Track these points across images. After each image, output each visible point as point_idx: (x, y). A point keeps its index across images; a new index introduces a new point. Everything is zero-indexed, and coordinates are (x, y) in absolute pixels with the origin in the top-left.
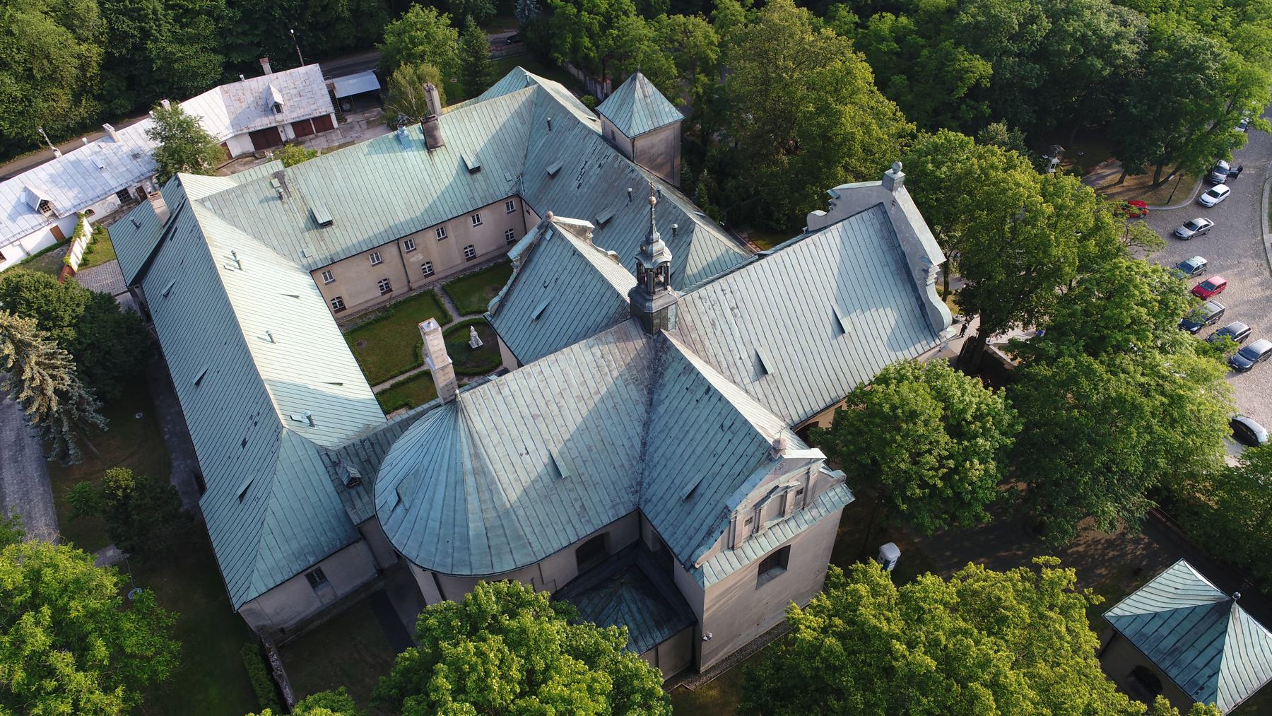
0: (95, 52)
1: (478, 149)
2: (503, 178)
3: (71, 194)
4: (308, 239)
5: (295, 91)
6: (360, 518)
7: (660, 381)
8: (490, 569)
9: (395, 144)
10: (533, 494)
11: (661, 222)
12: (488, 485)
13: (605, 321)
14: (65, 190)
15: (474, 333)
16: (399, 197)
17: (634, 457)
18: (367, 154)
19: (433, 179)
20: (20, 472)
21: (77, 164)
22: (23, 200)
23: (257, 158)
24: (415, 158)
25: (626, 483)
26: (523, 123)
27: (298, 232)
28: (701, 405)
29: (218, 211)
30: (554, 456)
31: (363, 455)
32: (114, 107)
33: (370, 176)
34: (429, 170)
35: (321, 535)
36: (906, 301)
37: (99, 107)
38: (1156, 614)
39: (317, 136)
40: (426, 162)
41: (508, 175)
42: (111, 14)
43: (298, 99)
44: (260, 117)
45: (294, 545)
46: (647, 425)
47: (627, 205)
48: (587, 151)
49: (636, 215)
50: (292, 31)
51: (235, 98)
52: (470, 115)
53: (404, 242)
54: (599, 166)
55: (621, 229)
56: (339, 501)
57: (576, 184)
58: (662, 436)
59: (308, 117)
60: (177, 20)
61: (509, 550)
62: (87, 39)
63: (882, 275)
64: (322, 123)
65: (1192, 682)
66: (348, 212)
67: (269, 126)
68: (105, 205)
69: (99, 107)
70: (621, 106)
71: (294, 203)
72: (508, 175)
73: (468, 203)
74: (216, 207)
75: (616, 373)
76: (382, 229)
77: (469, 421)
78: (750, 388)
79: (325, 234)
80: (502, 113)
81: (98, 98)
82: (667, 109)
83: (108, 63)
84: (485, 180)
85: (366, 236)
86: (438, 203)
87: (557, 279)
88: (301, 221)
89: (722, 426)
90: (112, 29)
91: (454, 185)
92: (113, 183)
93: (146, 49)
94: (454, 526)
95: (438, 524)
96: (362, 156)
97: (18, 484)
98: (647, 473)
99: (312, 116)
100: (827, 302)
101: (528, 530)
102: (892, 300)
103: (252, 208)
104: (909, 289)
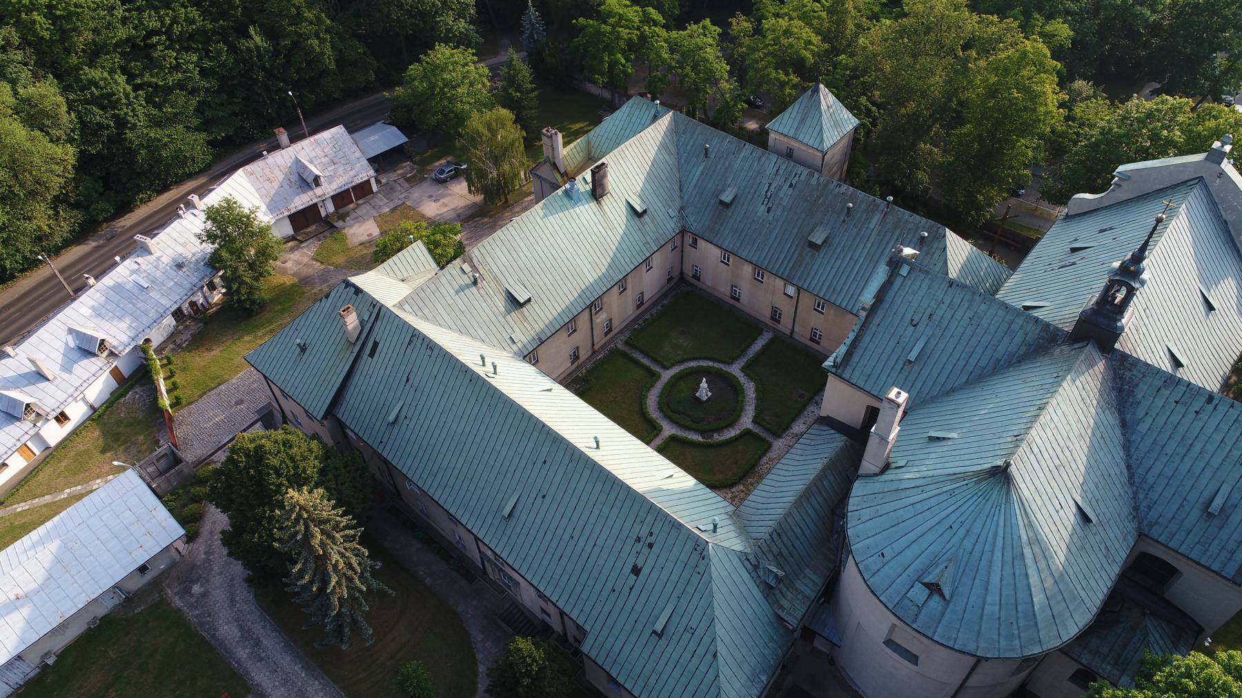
0: (69, 153)
3: (124, 325)
6: (794, 617)
7: (1131, 399)
8: (1059, 640)
9: (566, 200)
10: (1073, 549)
13: (1023, 349)
14: (115, 322)
15: (704, 385)
17: (1125, 483)
18: (544, 217)
19: (608, 230)
20: (276, 671)
21: (118, 288)
22: (72, 344)
23: (301, 242)
24: (586, 211)
26: (670, 154)
27: (501, 318)
28: (1204, 416)
29: (420, 313)
30: (1080, 504)
32: (94, 213)
33: (552, 240)
34: (602, 221)
35: (764, 649)
37: (79, 216)
39: (358, 205)
40: (598, 213)
42: (78, 105)
43: (333, 167)
44: (298, 194)
46: (1127, 446)
47: (844, 221)
50: (290, 93)
51: (264, 178)
53: (594, 307)
54: (791, 185)
55: (844, 246)
56: (768, 606)
57: (763, 209)
58: (1154, 455)
59: (346, 187)
60: (149, 100)
61: (1069, 614)
62: (59, 139)
64: (362, 190)
67: (311, 203)
68: (161, 330)
69: (79, 216)
70: (802, 121)
71: (487, 286)
72: (670, 211)
73: (644, 249)
74: (416, 308)
76: (576, 295)
77: (1019, 490)
79: (526, 313)
80: (651, 149)
81: (75, 206)
82: (846, 117)
83: (85, 163)
86: (619, 255)
87: (931, 315)
88: (500, 303)
90: (82, 122)
91: (627, 232)
92: (165, 302)
93: (126, 139)
94: (1017, 605)
95: (997, 608)
97: (283, 685)
98: (1141, 496)
100: (1196, 285)
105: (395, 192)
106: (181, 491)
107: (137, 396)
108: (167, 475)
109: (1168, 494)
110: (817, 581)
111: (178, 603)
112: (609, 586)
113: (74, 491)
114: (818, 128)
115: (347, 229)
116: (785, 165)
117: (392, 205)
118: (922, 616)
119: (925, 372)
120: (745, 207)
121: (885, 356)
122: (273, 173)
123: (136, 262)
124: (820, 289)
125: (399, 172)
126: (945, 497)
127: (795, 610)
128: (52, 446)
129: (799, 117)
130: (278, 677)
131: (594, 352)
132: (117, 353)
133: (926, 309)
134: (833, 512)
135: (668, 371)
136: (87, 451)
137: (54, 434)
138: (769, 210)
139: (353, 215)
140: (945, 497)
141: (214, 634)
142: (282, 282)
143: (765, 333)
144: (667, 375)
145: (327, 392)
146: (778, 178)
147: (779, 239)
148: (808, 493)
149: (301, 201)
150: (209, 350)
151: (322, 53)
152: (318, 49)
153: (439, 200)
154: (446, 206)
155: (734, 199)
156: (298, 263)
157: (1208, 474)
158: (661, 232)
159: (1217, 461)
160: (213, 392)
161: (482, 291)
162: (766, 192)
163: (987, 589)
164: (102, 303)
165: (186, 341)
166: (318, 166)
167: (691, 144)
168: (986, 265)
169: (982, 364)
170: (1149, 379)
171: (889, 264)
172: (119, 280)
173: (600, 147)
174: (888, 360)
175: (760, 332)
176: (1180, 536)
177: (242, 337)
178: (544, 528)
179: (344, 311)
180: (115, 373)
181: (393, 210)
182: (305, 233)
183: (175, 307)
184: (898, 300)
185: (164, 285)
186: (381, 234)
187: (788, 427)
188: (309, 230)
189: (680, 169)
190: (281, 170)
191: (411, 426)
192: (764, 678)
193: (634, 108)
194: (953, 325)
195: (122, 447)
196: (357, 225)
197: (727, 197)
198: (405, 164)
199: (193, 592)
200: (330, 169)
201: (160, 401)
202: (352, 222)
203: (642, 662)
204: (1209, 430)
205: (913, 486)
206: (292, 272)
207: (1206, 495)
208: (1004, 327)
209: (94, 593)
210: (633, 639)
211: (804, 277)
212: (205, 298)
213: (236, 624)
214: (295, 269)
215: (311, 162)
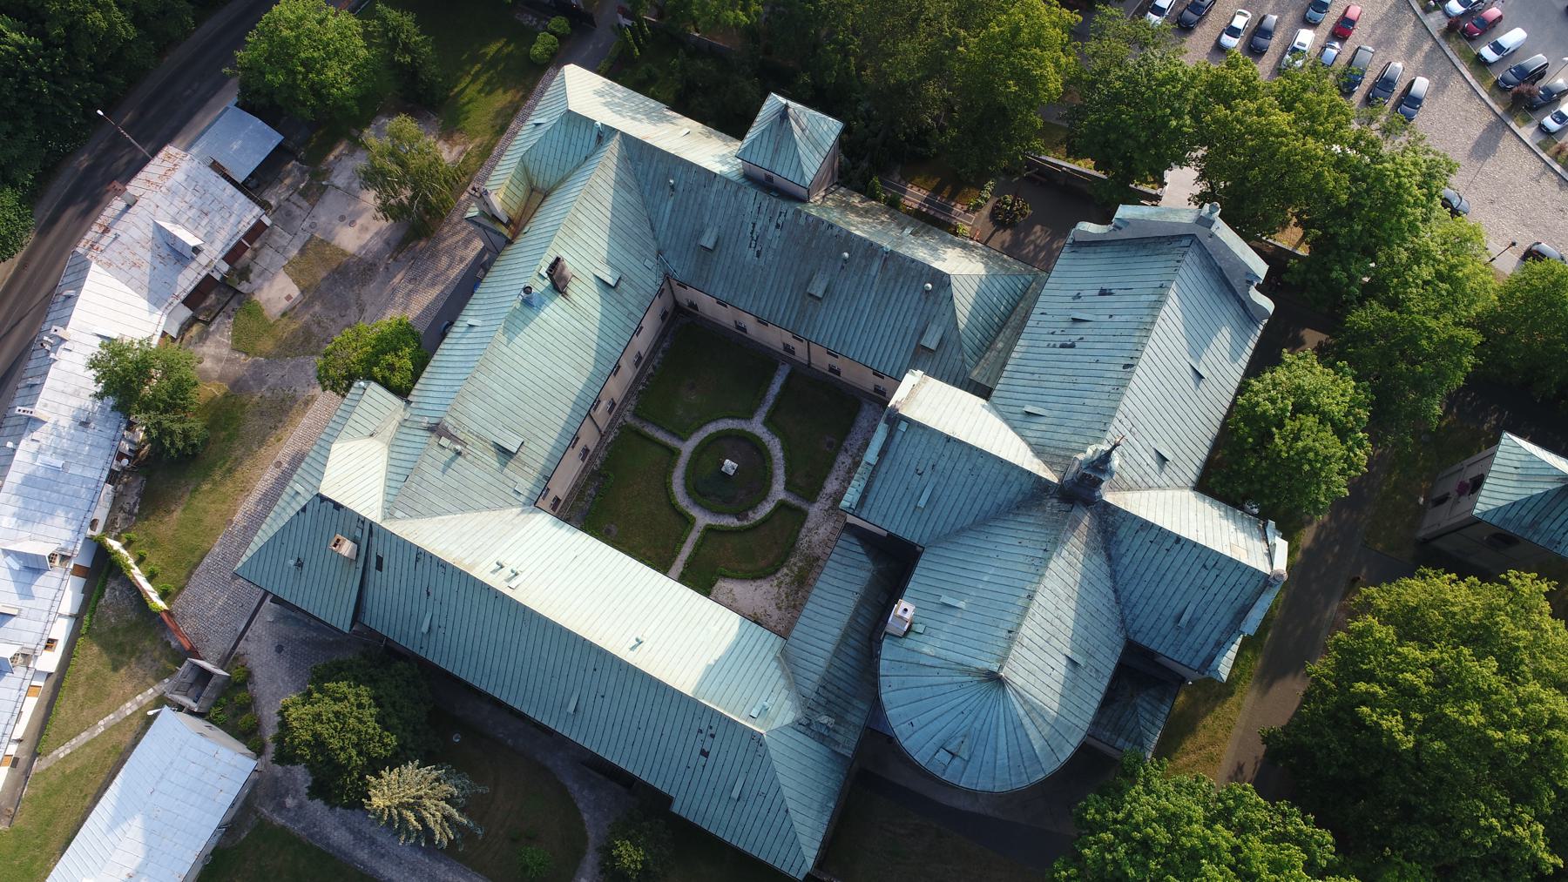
1: (605, 254)
2: (644, 270)
4: (511, 474)
5: (194, 211)
6: (849, 748)
7: (1115, 539)
9: (527, 311)
11: (901, 280)
12: (1033, 709)
13: (1020, 497)
14: (49, 521)
16: (564, 366)
21: (29, 480)
23: (208, 324)
25: (1114, 628)
27: (498, 475)
28: (1173, 553)
29: (414, 513)
31: (822, 701)
33: (525, 364)
36: (1232, 310)
38: (1515, 503)
41: (648, 263)
45: (816, 806)
46: (1113, 576)
47: (843, 267)
48: (749, 210)
49: (861, 277)
50: (100, 112)
52: (576, 221)
54: (778, 226)
55: (847, 296)
57: (751, 253)
58: (1136, 581)
59: (237, 238)
63: (1211, 302)
65: (1551, 541)
66: (529, 418)
67: (200, 278)
70: (776, 151)
72: (648, 263)
73: (628, 322)
75: (1081, 558)
76: (568, 411)
78: (1161, 483)
80: (605, 195)
84: (630, 285)
85: (559, 429)
86: (603, 343)
88: (492, 460)
89: (1204, 566)
91: (606, 313)
95: (1006, 761)
96: (505, 350)
97: (413, 875)
98: (1127, 612)
99: (242, 234)
101: (1072, 719)
102: (1223, 319)
103: (440, 485)
104: (1231, 297)
105: (294, 218)
106: (224, 700)
107: (117, 593)
108: (204, 694)
109: (1148, 610)
110: (865, 708)
111: (279, 820)
112: (684, 764)
113: (108, 722)
114: (795, 160)
115: (257, 293)
116: (767, 201)
117: (298, 243)
118: (948, 770)
119: (935, 514)
120: (730, 251)
121: (897, 500)
122: (135, 254)
123: (33, 440)
124: (829, 342)
125: (287, 181)
126: (955, 687)
127: (848, 742)
128: (53, 671)
129: (771, 146)
130: (405, 868)
131: (602, 436)
132: (69, 554)
133: (928, 460)
134: (870, 639)
135: (687, 443)
136: (96, 672)
137: (49, 661)
138: (758, 254)
139: (256, 270)
140: (955, 687)
141: (328, 843)
142: (211, 395)
143: (781, 367)
144: (687, 448)
145: (344, 607)
146: (762, 216)
147: (776, 287)
148: (845, 636)
149: (187, 280)
150: (169, 512)
151: (112, 25)
152: (104, 25)
153: (354, 221)
154: (367, 229)
155: (716, 243)
156: (218, 359)
157: (1178, 595)
158: (643, 292)
159: (1184, 586)
160: (200, 568)
161: (469, 457)
162: (752, 233)
163: (996, 752)
164: (22, 506)
165: (135, 504)
166: (186, 224)
167: (652, 173)
168: (998, 287)
169: (986, 508)
170: (1128, 523)
171: (886, 422)
172: (27, 471)
173: (545, 159)
174: (900, 503)
175: (774, 367)
176: (1158, 640)
177: (199, 485)
178: (611, 720)
179: (335, 545)
180: (78, 571)
181: (302, 252)
182: (206, 309)
183: (105, 474)
184: (901, 452)
185: (80, 454)
186: (302, 292)
187: (821, 487)
188: (208, 302)
189: (645, 205)
190: (143, 247)
191: (448, 634)
192: (832, 805)
193: (571, 124)
194: (955, 475)
195: (133, 659)
196: (266, 285)
197: (708, 241)
198: (289, 166)
199: (288, 806)
200: (203, 223)
201: (150, 605)
202: (260, 281)
203: (726, 818)
204: (1177, 563)
205: (930, 664)
206: (215, 375)
207: (1177, 611)
208: (1001, 478)
209: (198, 846)
210: (715, 801)
211: (811, 329)
212: (131, 442)
213: (344, 828)
214: (218, 369)
215: (175, 221)
